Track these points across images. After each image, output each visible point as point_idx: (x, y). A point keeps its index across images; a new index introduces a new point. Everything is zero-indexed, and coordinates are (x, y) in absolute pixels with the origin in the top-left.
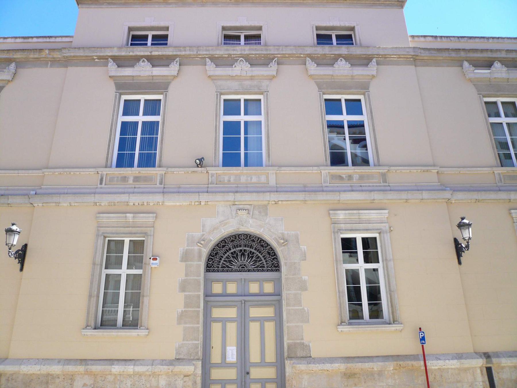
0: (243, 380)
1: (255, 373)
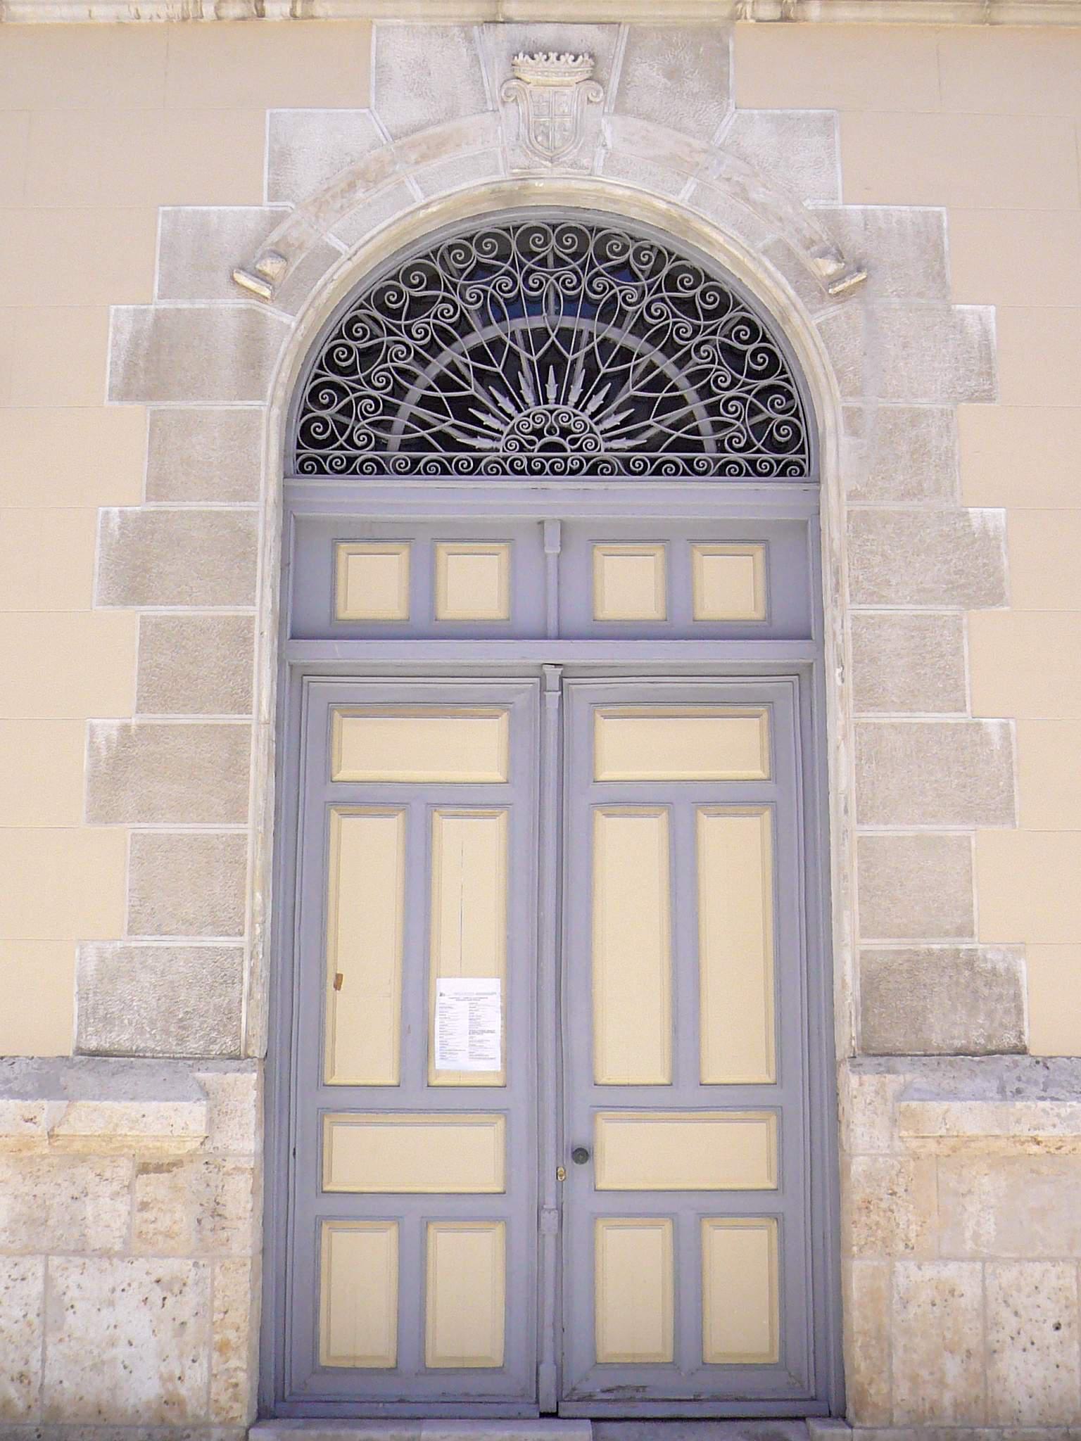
0: (550, 1202)
1: (633, 1154)
